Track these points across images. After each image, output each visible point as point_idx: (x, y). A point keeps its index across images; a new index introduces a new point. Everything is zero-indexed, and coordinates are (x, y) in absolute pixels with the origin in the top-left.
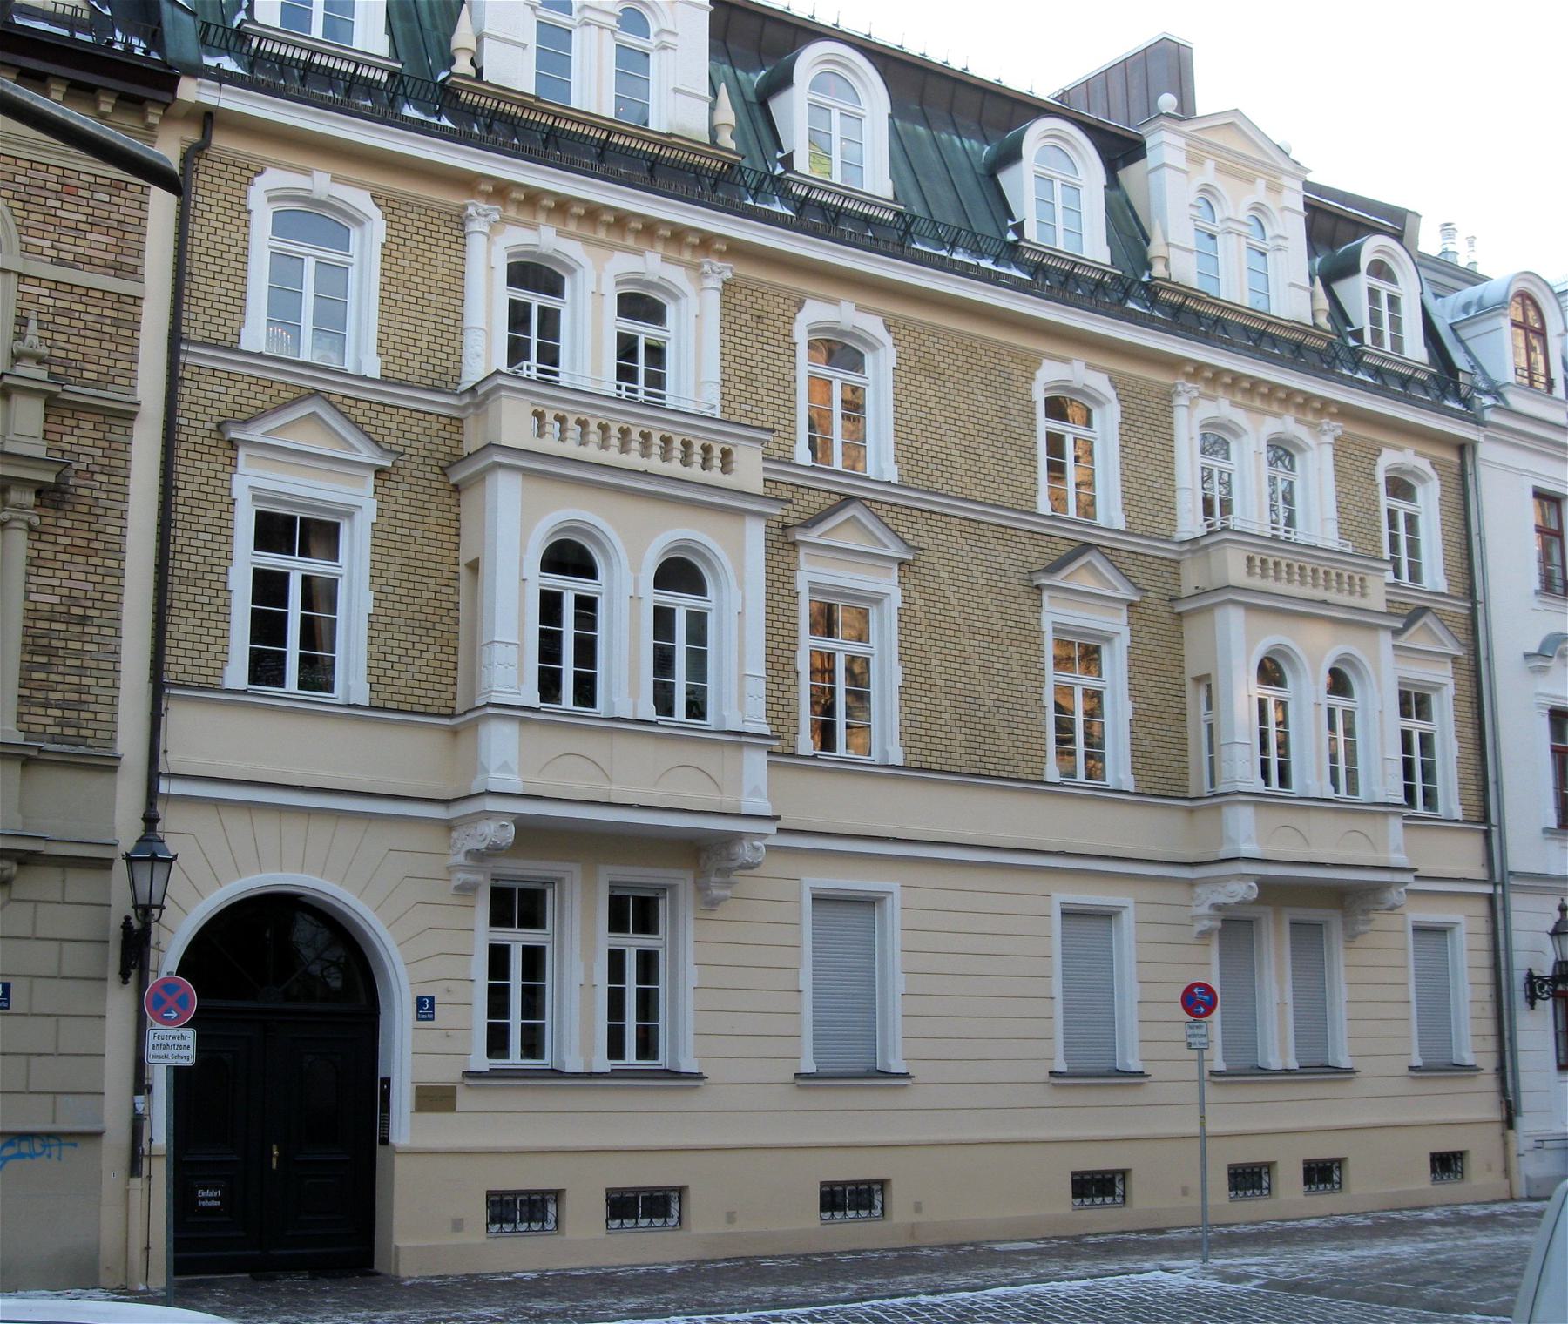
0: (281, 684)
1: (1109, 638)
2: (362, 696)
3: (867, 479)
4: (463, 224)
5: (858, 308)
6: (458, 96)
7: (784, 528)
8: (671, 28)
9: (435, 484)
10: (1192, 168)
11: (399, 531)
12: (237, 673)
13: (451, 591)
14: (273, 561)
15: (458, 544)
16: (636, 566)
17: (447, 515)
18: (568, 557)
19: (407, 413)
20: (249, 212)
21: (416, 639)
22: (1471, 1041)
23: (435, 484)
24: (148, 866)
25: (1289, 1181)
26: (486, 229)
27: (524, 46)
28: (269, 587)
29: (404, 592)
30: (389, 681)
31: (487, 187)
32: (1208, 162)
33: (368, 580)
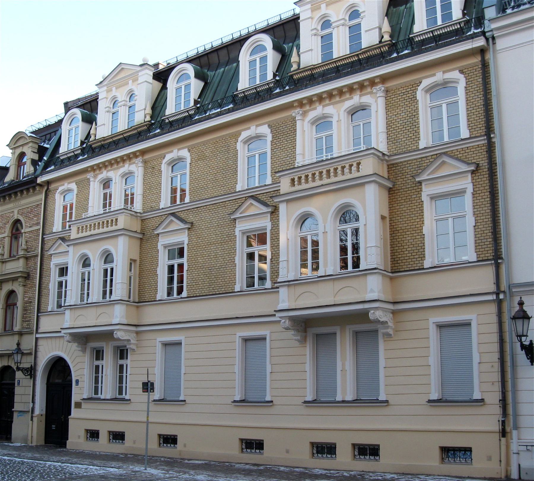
3: (55, 233)
22: (483, 383)
24: (521, 320)
25: (104, 437)
28: (171, 269)
31: (296, 104)
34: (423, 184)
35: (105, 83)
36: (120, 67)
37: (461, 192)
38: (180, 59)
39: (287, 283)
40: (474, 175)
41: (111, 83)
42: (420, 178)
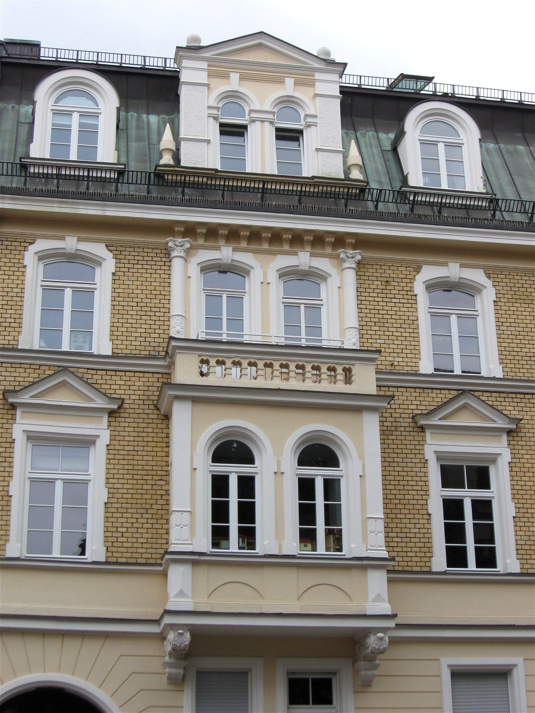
0: (465, 565)
1: (493, 458)
2: (515, 567)
4: (169, 254)
5: (462, 266)
6: (164, 178)
7: (413, 417)
8: (313, 112)
9: (151, 416)
10: (214, 82)
11: (127, 448)
12: (439, 561)
13: (163, 483)
14: (453, 493)
15: (168, 452)
16: (278, 452)
17: (160, 435)
18: (232, 450)
19: (132, 374)
20: (25, 267)
21: (139, 516)
23: (151, 416)
26: (182, 254)
27: (208, 142)
28: (453, 508)
29: (130, 486)
30: (120, 544)
32: (232, 75)
33: (103, 480)
34: (19, 412)
35: (208, 55)
36: (260, 40)
37: (88, 442)
38: (84, 58)
39: (197, 557)
40: (112, 419)
41: (214, 59)
42: (17, 398)
